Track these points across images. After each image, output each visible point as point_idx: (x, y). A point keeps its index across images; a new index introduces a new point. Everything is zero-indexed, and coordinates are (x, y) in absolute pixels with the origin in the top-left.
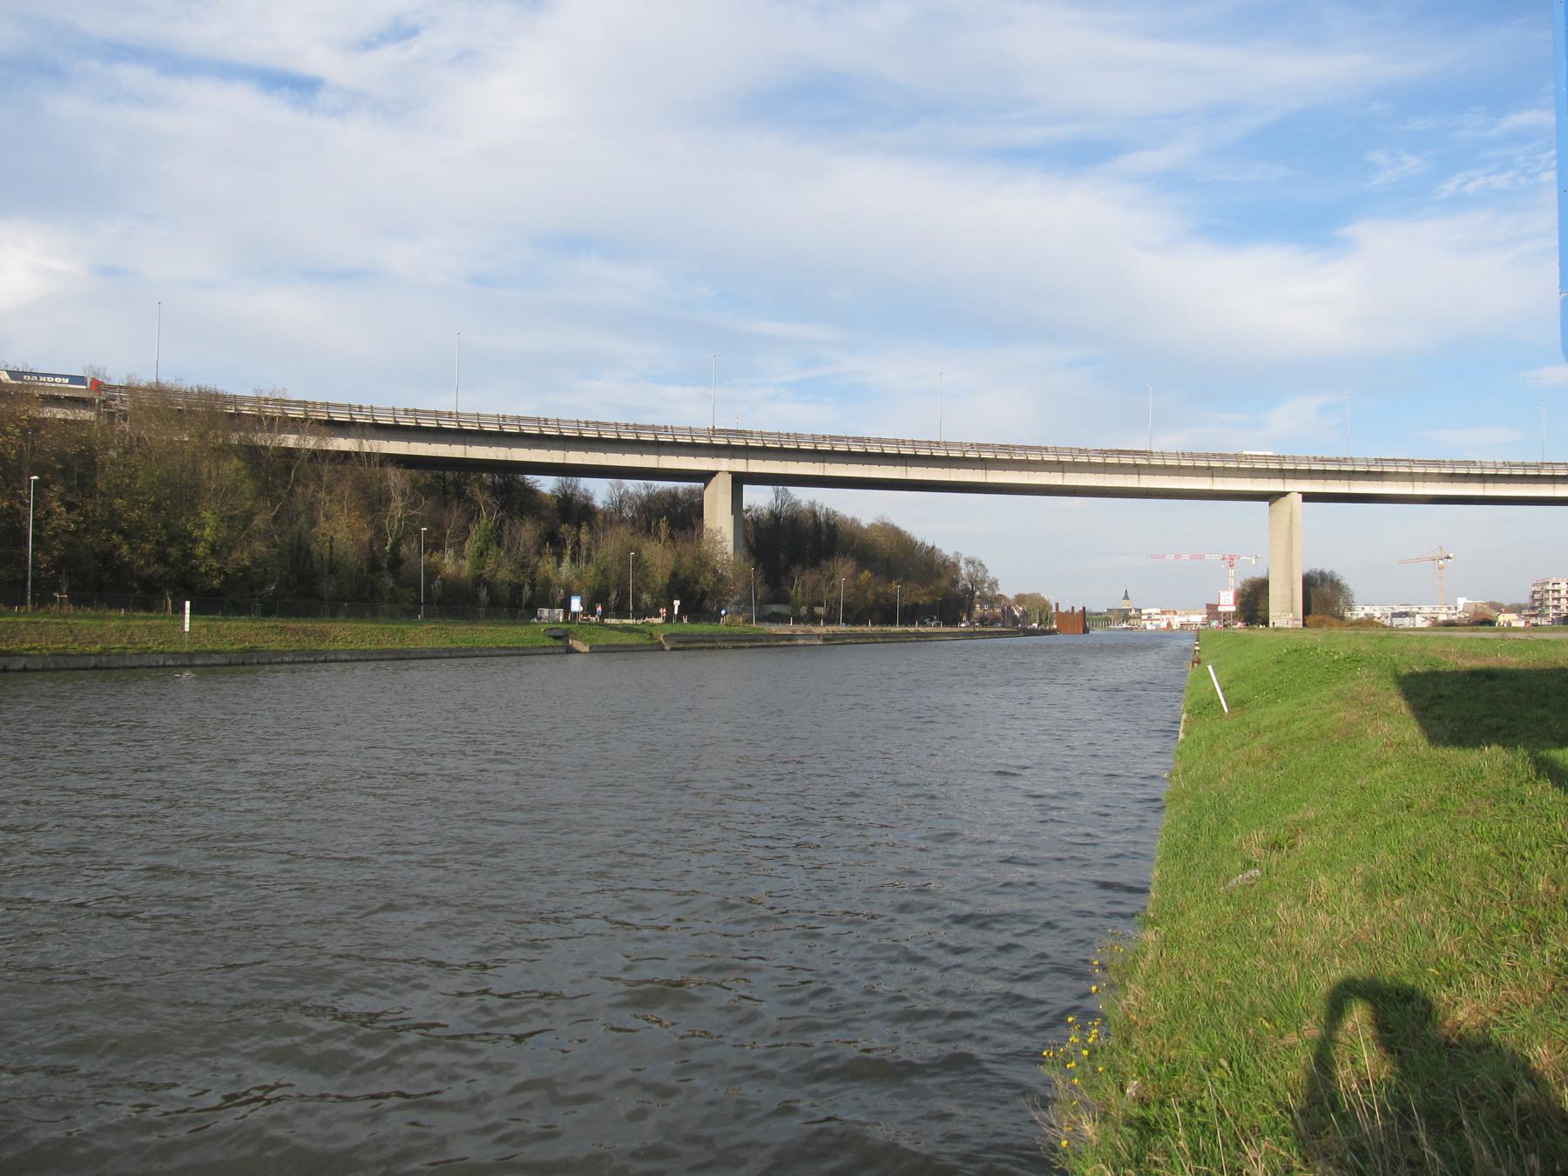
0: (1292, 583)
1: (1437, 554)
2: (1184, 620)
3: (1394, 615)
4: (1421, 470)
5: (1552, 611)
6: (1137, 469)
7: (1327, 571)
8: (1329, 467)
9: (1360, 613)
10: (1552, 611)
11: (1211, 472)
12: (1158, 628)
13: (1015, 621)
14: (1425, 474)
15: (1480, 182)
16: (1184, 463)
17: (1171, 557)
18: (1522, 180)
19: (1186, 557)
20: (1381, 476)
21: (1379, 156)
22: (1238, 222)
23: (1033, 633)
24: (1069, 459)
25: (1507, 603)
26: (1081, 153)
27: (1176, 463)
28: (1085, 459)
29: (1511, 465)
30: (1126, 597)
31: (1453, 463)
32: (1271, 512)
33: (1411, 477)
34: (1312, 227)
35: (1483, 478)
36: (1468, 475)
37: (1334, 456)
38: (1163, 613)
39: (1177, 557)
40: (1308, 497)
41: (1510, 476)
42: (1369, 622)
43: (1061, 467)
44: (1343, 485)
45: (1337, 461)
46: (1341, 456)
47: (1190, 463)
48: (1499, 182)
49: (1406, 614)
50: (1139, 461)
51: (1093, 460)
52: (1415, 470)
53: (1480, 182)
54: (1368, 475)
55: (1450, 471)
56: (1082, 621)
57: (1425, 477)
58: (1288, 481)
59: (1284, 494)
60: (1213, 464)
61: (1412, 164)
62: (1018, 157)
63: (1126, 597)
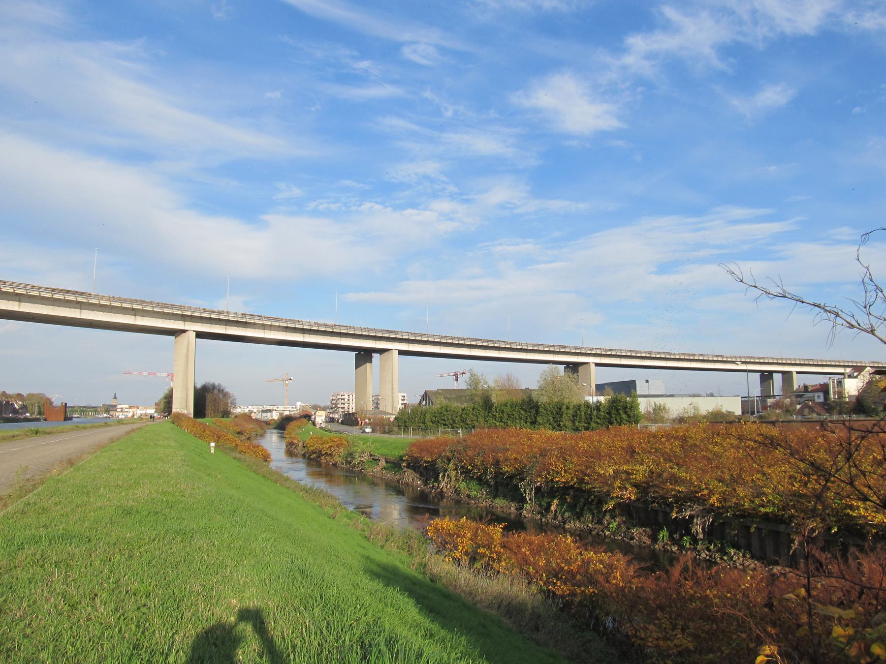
0: (187, 390)
1: (285, 377)
2: (143, 412)
3: (263, 411)
4: (269, 323)
5: (340, 410)
6: (80, 305)
7: (216, 384)
8: (213, 316)
9: (238, 410)
10: (340, 410)
11: (134, 312)
12: (126, 417)
13: (15, 411)
14: (271, 326)
15: (325, 206)
16: (114, 304)
17: (135, 373)
18: (343, 208)
19: (145, 373)
20: (245, 325)
21: (282, 185)
22: (210, 203)
23: (27, 420)
24: (24, 292)
25: (322, 405)
26: (136, 154)
27: (108, 303)
28: (37, 294)
29: (319, 325)
30: (115, 398)
31: (287, 321)
32: (176, 342)
33: (264, 327)
34: (249, 212)
35: (303, 331)
36: (295, 328)
37: (216, 310)
38: (130, 408)
39: (140, 373)
40: (200, 335)
41: (318, 331)
42: (247, 417)
43: (19, 298)
44: (222, 331)
45: (218, 312)
46: (221, 310)
47: (119, 305)
48: (334, 207)
49: (269, 411)
50: (80, 299)
51: (43, 294)
52: (265, 323)
53: (325, 206)
54: (237, 323)
55: (285, 325)
56: (66, 414)
57: (271, 328)
58: (187, 323)
59: (184, 331)
60: (135, 307)
61: (297, 192)
62: (97, 151)
63: (115, 398)
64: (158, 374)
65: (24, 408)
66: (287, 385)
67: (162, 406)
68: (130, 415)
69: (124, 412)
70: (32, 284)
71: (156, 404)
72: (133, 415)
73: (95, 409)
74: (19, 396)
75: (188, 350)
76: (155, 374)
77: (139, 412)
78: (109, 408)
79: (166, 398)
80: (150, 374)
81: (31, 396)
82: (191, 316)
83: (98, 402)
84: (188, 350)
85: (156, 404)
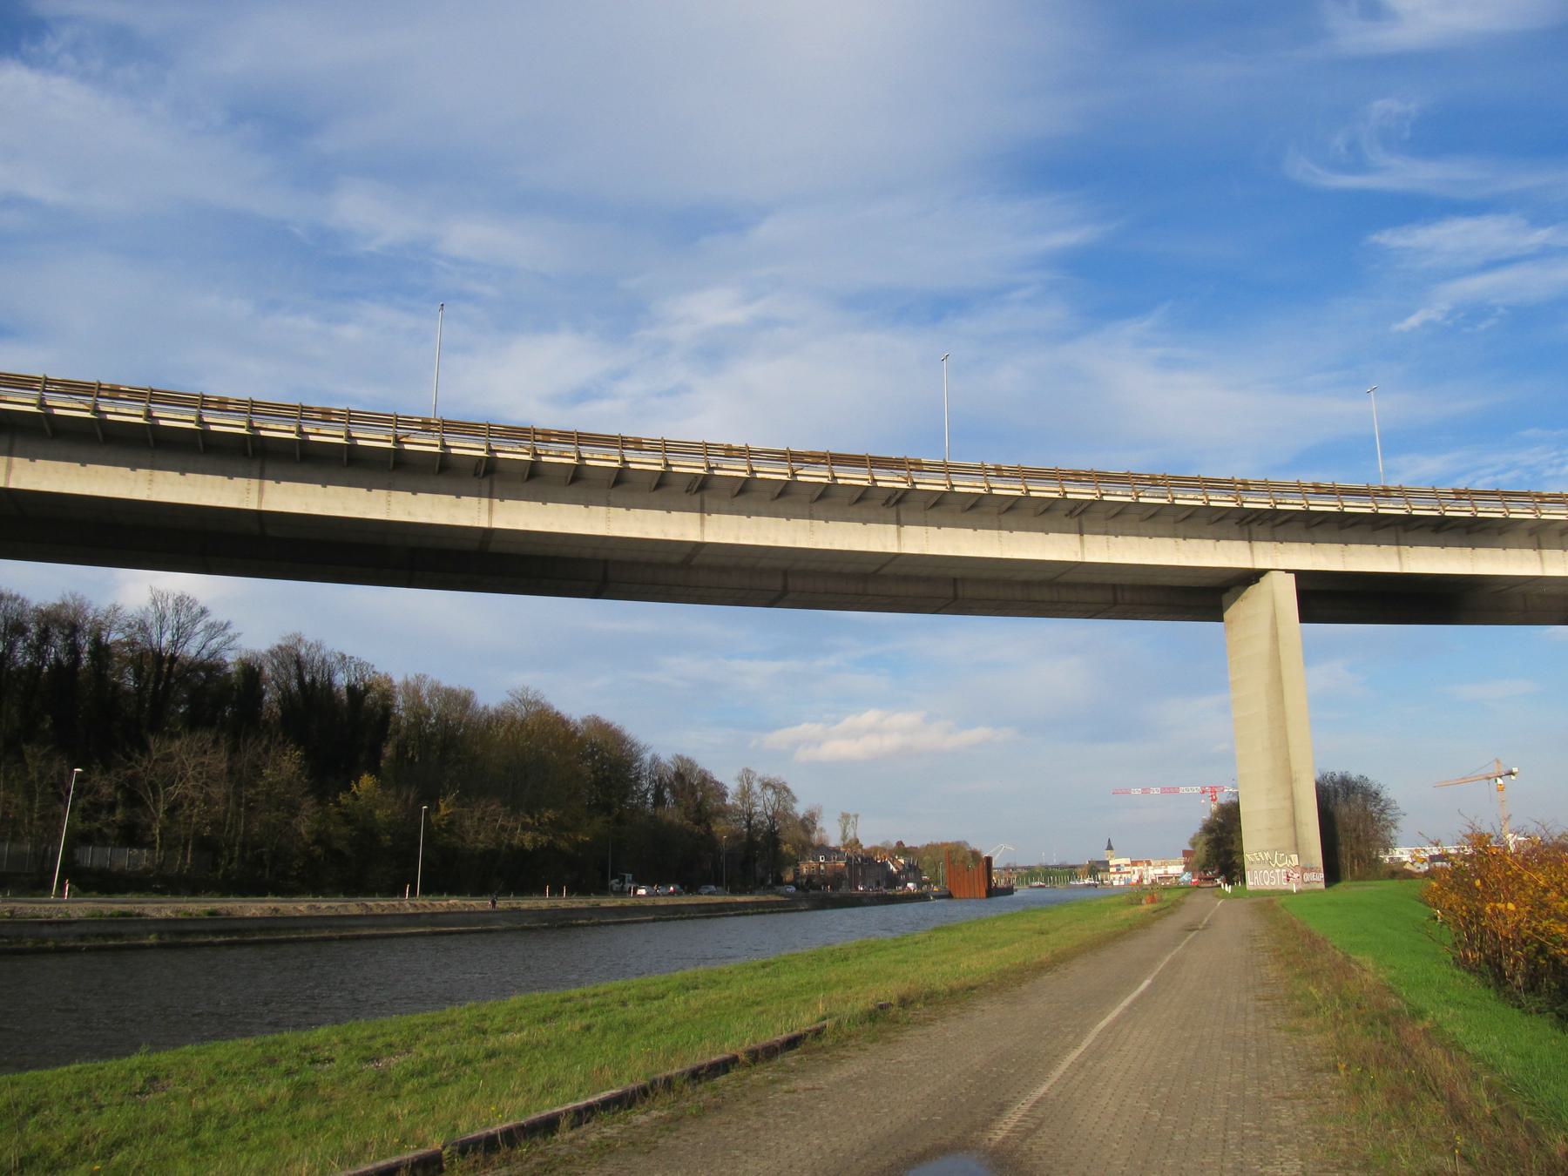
2: (1161, 871)
12: (1128, 882)
17: (1137, 791)
19: (1155, 791)
30: (1110, 848)
38: (1134, 864)
39: (1145, 791)
64: (1183, 790)
65: (913, 870)
66: (1501, 789)
67: (1201, 852)
68: (1135, 878)
69: (1124, 873)
70: (725, 442)
71: (1186, 853)
72: (1141, 880)
73: (1071, 871)
74: (901, 849)
75: (1275, 637)
76: (1175, 791)
77: (1152, 873)
78: (1097, 868)
79: (1208, 828)
80: (1164, 791)
81: (932, 849)
82: (1275, 513)
83: (1080, 858)
84: (1275, 637)
85: (1186, 853)
